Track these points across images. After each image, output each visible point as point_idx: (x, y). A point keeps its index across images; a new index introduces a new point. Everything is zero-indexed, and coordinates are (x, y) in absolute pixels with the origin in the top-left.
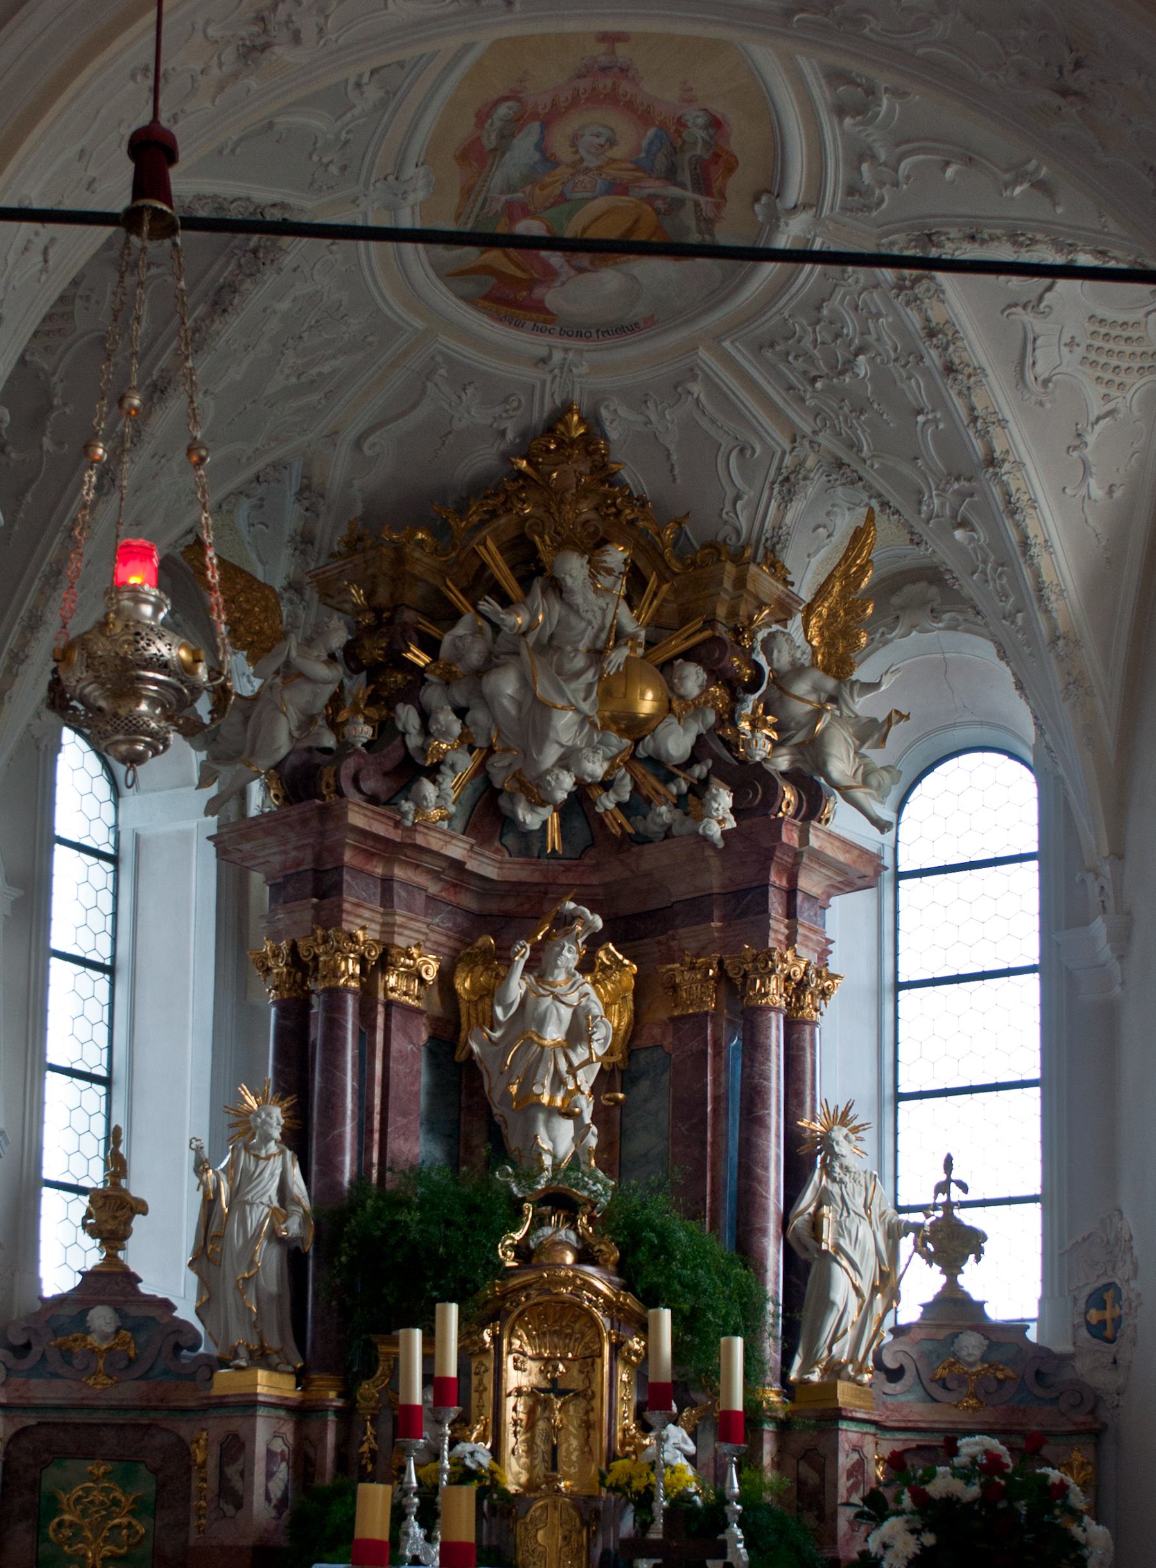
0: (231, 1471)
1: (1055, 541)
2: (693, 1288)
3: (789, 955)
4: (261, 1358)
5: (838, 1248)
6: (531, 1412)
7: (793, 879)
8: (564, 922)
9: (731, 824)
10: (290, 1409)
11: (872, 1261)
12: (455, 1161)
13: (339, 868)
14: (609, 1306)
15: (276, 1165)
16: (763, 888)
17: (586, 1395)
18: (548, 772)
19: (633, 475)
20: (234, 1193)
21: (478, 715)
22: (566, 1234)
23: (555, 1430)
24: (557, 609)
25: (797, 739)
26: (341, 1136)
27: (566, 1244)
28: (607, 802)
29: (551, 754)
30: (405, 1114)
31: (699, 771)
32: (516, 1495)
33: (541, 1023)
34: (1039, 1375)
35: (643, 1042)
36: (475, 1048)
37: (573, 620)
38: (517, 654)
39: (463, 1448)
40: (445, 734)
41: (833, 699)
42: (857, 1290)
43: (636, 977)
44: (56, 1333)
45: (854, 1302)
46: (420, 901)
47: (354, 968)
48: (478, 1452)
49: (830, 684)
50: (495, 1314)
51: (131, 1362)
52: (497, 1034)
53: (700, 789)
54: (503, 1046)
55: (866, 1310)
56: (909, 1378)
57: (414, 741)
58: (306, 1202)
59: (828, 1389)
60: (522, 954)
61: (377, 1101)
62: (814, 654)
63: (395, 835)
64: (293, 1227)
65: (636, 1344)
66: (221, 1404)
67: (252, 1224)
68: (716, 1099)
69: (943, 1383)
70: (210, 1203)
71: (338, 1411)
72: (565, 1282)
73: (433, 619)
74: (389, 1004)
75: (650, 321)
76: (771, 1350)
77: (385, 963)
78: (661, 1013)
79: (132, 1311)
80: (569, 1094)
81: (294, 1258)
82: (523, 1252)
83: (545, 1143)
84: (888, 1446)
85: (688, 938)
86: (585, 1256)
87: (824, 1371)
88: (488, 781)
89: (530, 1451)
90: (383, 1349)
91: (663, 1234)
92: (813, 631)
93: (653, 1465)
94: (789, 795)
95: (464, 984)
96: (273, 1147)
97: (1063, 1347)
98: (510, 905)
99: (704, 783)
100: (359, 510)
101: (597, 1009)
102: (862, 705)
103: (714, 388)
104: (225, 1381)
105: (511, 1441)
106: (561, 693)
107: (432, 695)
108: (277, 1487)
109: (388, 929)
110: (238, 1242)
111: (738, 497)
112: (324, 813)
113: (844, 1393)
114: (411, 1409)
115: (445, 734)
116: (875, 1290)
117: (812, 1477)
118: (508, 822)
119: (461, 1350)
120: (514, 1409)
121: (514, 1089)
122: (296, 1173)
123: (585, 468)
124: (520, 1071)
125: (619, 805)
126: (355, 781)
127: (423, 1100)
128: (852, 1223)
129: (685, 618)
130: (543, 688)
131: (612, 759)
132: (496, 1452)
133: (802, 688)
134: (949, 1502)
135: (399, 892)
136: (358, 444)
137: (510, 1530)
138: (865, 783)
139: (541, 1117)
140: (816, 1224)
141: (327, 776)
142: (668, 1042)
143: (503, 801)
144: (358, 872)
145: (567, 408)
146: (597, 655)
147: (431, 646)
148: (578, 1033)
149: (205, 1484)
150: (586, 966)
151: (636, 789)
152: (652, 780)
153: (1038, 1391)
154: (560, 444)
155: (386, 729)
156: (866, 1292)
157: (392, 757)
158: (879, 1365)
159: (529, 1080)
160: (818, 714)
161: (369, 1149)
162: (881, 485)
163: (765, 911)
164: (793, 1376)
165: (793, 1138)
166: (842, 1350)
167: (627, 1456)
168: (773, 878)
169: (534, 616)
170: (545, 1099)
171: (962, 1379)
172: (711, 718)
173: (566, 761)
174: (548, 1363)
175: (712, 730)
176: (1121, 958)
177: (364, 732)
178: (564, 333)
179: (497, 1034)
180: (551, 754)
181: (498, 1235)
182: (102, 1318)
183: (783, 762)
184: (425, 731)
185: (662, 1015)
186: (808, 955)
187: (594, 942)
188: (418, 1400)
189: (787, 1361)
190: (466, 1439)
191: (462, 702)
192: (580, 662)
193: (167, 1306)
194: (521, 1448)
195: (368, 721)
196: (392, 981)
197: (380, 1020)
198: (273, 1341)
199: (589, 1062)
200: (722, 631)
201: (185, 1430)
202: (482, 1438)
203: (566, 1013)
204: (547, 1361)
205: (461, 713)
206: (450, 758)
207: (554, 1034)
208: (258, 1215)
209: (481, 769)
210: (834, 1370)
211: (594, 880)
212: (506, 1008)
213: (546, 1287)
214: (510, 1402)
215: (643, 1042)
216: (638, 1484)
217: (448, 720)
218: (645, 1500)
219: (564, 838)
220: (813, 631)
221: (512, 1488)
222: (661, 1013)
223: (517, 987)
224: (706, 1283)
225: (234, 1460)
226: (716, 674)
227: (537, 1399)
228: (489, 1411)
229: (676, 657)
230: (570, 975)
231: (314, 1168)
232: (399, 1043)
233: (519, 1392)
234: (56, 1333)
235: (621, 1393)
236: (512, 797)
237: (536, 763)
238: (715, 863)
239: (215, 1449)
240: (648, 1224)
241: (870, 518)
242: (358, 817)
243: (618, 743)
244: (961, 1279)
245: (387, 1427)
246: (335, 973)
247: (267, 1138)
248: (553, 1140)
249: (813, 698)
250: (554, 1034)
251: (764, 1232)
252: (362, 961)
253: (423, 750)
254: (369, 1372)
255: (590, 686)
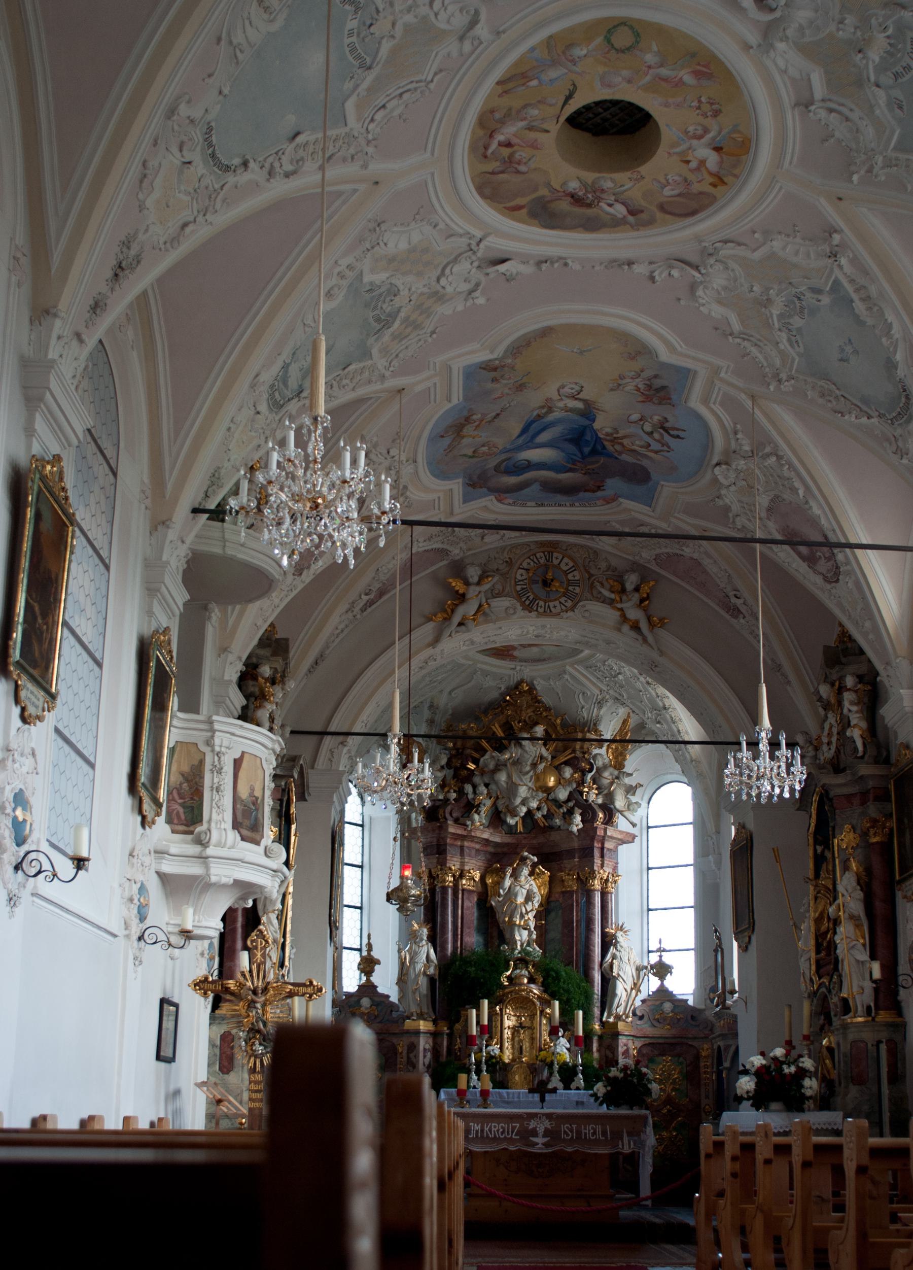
0: (411, 1055)
1: (689, 731)
2: (567, 991)
3: (601, 871)
4: (421, 1016)
5: (619, 975)
6: (513, 1034)
7: (603, 844)
8: (523, 860)
9: (581, 826)
10: (431, 1034)
11: (631, 979)
12: (487, 944)
13: (446, 844)
14: (539, 998)
15: (425, 949)
16: (592, 849)
17: (531, 1028)
18: (517, 806)
19: (546, 699)
20: (411, 959)
21: (493, 787)
22: (525, 972)
23: (521, 1041)
24: (520, 751)
25: (606, 792)
26: (447, 938)
27: (524, 976)
28: (539, 815)
29: (518, 801)
30: (469, 928)
31: (571, 804)
32: (509, 1064)
33: (516, 895)
34: (693, 1018)
35: (552, 899)
36: (493, 903)
37: (525, 755)
38: (506, 765)
39: (490, 1048)
40: (482, 794)
41: (617, 778)
42: (626, 990)
43: (550, 877)
44: (350, 1007)
45: (624, 993)
46: (473, 852)
47: (451, 879)
48: (495, 1049)
49: (616, 773)
50: (500, 1001)
51: (376, 1017)
52: (501, 899)
53: (570, 812)
54: (502, 904)
55: (629, 996)
56: (646, 1018)
57: (470, 796)
58: (435, 961)
59: (615, 1024)
60: (509, 871)
61: (459, 924)
62: (611, 760)
63: (465, 833)
64: (431, 971)
65: (548, 1011)
66: (408, 1032)
67: (417, 970)
68: (577, 921)
69: (658, 1020)
70: (402, 964)
71: (447, 1034)
72: (524, 990)
73: (476, 750)
74: (463, 890)
75: (549, 659)
76: (597, 1011)
77: (462, 876)
78: (558, 889)
79: (376, 999)
80: (526, 921)
81: (432, 980)
82: (509, 978)
83: (518, 938)
84: (639, 1044)
85: (567, 863)
86: (531, 980)
87: (615, 1017)
88: (497, 809)
89: (513, 1048)
90: (463, 1012)
91: (557, 972)
92: (610, 754)
93: (553, 1053)
94: (601, 815)
95: (489, 881)
96: (424, 942)
97: (703, 1007)
98: (505, 850)
99: (573, 808)
100: (450, 712)
101: (535, 890)
102: (627, 781)
103: (573, 677)
104: (409, 1024)
105: (506, 1044)
106: (522, 780)
107: (477, 779)
108: (427, 1061)
109: (462, 864)
110: (413, 976)
111: (583, 708)
112: (440, 828)
113: (621, 1026)
114: (473, 1037)
115: (482, 794)
116: (632, 989)
117: (610, 1055)
118: (504, 822)
119: (489, 1013)
120: (507, 1033)
121: (507, 919)
122: (432, 951)
123: (530, 698)
124: (509, 913)
125: (543, 816)
126: (451, 814)
127: (475, 922)
128: (623, 966)
129: (565, 750)
130: (515, 779)
131: (540, 800)
132: (501, 1048)
133: (606, 774)
134: (615, 1078)
135: (466, 851)
136: (450, 693)
137: (507, 1076)
138: (629, 809)
139: (516, 928)
140: (611, 966)
141: (441, 811)
142: (561, 900)
143: (502, 815)
144: (451, 845)
145: (522, 681)
146: (534, 765)
147: (476, 762)
148: (529, 898)
149: (402, 1060)
150: (531, 874)
151: (549, 810)
152: (554, 807)
153: (692, 1022)
154: (520, 692)
155: (461, 792)
156: (629, 991)
157: (463, 802)
158: (634, 1014)
159: (511, 916)
160: (612, 783)
161: (457, 941)
162: (631, 706)
163: (593, 856)
164: (604, 1019)
165: (604, 935)
166: (620, 1011)
167: (545, 1049)
168: (596, 844)
169: (512, 754)
170: (518, 923)
171: (665, 1019)
172: (574, 786)
173: (524, 802)
174: (519, 1017)
175: (574, 790)
176: (719, 869)
177: (453, 795)
178: (521, 661)
179: (501, 899)
180: (518, 801)
181: (501, 974)
182: (365, 1002)
183: (600, 801)
184: (475, 792)
185: (559, 890)
186: (608, 869)
187: (534, 865)
188: (474, 1033)
189: (602, 1014)
190: (491, 1045)
191: (487, 781)
192: (528, 768)
193: (388, 997)
194: (510, 1047)
195: (455, 791)
196: (464, 882)
197: (460, 896)
198: (425, 1010)
199: (532, 910)
200: (579, 754)
201: (395, 1041)
202: (497, 1044)
203: (525, 892)
204: (518, 1017)
205: (487, 785)
206: (484, 802)
207: (520, 899)
208: (420, 966)
209: (494, 805)
210: (618, 1017)
211: (535, 842)
212: (504, 890)
213: (517, 992)
214: (506, 1031)
215: (551, 899)
216: (548, 1060)
217: (483, 789)
218: (551, 1065)
219: (523, 826)
220: (610, 754)
221: (507, 1061)
222: (558, 889)
223: (508, 882)
224: (572, 989)
225: (412, 1051)
226: (576, 768)
227: (515, 1030)
228: (499, 1034)
229: (562, 764)
230: (526, 878)
231: (438, 949)
232: (467, 903)
233: (509, 1027)
234: (350, 1007)
235: (544, 1027)
236: (505, 814)
237: (513, 803)
238: (576, 839)
239: (406, 1048)
240: (552, 969)
241: (629, 716)
242: (451, 830)
243: (541, 795)
244: (665, 982)
245: (464, 1040)
246: (444, 881)
247: (422, 940)
248: (521, 936)
249: (610, 777)
250: (520, 899)
251: (593, 969)
252: (454, 876)
253: (474, 799)
254: (458, 1021)
255: (531, 777)
